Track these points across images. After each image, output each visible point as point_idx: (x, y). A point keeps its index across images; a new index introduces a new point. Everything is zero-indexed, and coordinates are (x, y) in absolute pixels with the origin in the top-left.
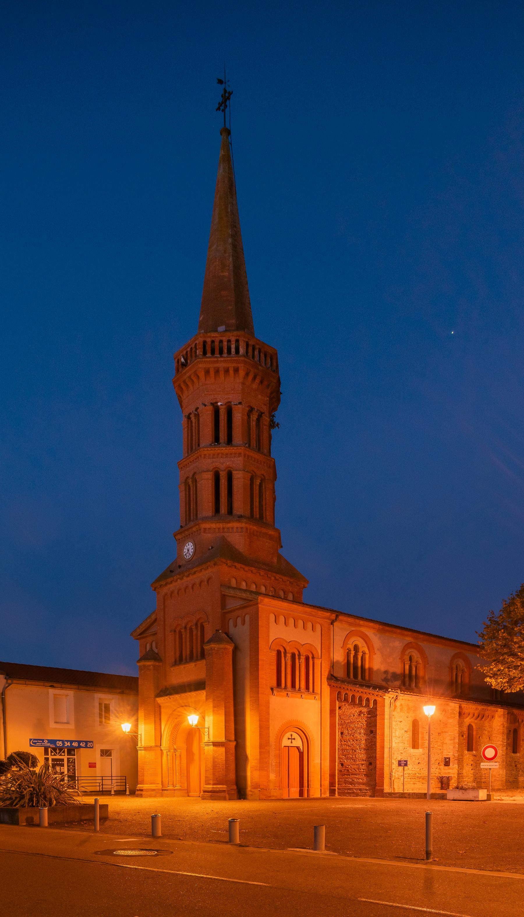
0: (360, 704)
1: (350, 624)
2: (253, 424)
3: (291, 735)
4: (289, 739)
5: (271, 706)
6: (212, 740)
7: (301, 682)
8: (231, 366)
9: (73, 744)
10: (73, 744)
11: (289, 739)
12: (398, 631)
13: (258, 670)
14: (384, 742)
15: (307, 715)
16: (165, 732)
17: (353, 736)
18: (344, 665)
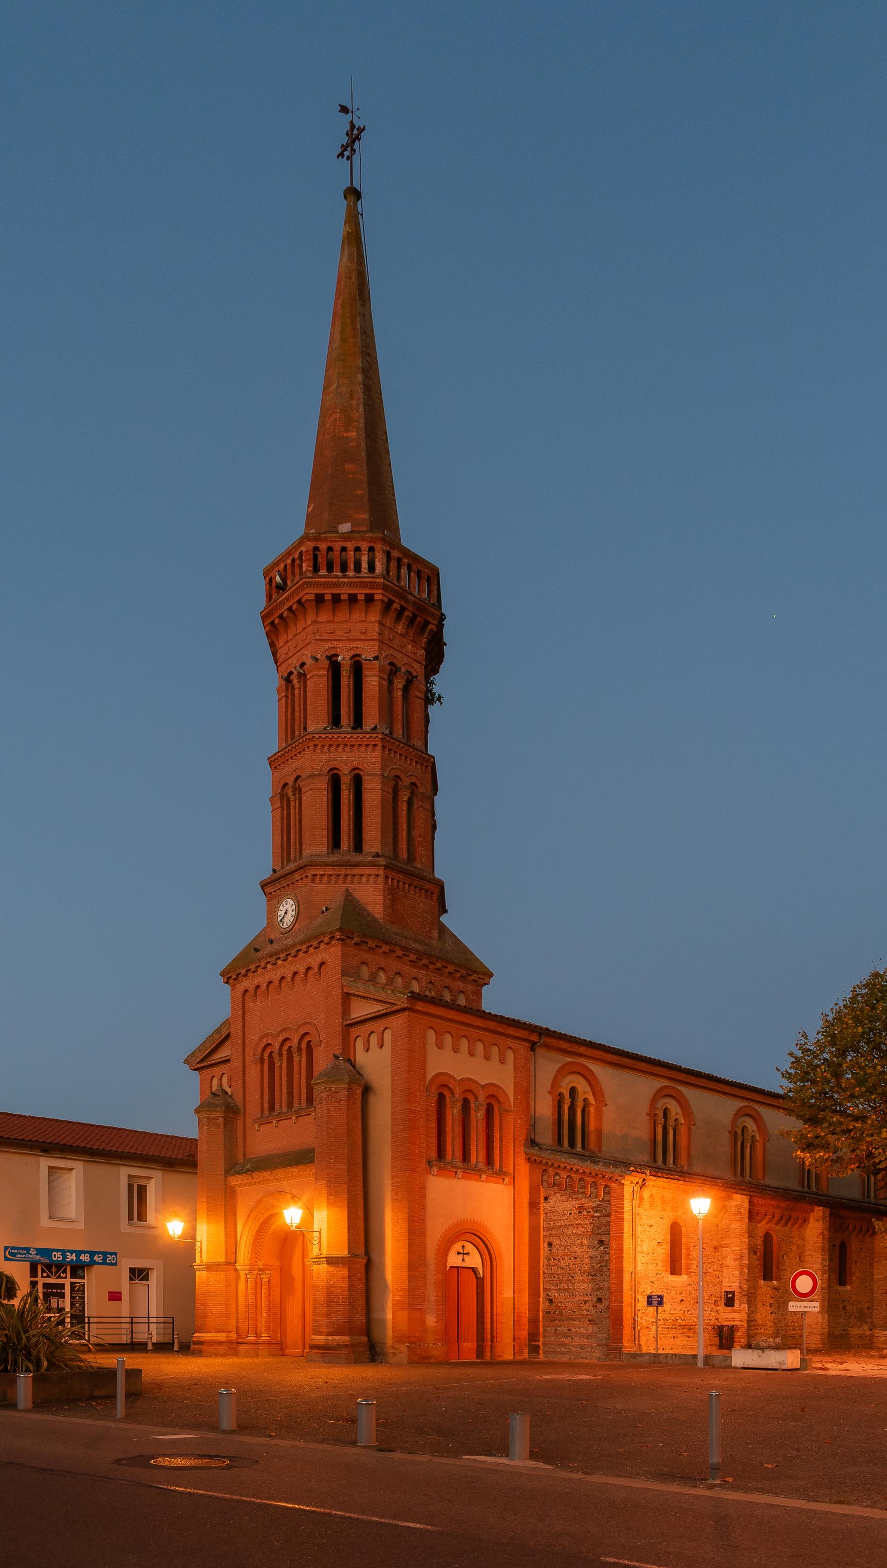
3: (463, 1247)
4: (459, 1253)
6: (325, 1252)
8: (361, 593)
11: (459, 1253)
16: (244, 1239)
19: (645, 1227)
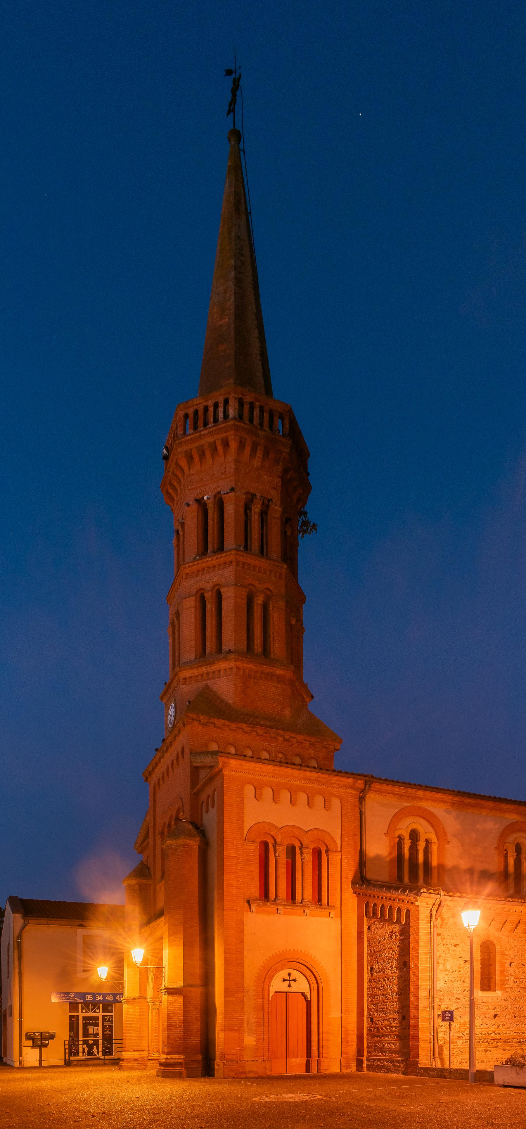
0: (390, 920)
1: (400, 796)
2: (255, 518)
3: (289, 974)
4: (284, 980)
5: (246, 929)
7: (305, 889)
9: (107, 998)
10: (107, 998)
11: (284, 980)
12: (490, 804)
13: (223, 874)
14: (418, 981)
15: (318, 940)
17: (384, 972)
18: (391, 861)
19: (449, 946)
